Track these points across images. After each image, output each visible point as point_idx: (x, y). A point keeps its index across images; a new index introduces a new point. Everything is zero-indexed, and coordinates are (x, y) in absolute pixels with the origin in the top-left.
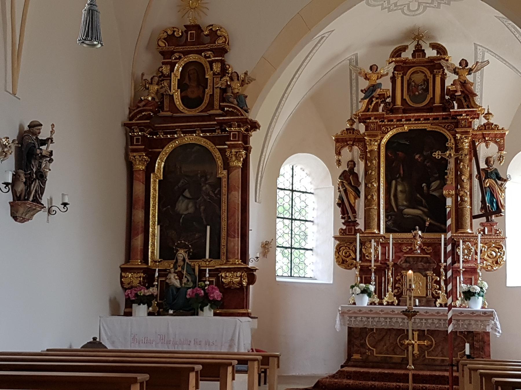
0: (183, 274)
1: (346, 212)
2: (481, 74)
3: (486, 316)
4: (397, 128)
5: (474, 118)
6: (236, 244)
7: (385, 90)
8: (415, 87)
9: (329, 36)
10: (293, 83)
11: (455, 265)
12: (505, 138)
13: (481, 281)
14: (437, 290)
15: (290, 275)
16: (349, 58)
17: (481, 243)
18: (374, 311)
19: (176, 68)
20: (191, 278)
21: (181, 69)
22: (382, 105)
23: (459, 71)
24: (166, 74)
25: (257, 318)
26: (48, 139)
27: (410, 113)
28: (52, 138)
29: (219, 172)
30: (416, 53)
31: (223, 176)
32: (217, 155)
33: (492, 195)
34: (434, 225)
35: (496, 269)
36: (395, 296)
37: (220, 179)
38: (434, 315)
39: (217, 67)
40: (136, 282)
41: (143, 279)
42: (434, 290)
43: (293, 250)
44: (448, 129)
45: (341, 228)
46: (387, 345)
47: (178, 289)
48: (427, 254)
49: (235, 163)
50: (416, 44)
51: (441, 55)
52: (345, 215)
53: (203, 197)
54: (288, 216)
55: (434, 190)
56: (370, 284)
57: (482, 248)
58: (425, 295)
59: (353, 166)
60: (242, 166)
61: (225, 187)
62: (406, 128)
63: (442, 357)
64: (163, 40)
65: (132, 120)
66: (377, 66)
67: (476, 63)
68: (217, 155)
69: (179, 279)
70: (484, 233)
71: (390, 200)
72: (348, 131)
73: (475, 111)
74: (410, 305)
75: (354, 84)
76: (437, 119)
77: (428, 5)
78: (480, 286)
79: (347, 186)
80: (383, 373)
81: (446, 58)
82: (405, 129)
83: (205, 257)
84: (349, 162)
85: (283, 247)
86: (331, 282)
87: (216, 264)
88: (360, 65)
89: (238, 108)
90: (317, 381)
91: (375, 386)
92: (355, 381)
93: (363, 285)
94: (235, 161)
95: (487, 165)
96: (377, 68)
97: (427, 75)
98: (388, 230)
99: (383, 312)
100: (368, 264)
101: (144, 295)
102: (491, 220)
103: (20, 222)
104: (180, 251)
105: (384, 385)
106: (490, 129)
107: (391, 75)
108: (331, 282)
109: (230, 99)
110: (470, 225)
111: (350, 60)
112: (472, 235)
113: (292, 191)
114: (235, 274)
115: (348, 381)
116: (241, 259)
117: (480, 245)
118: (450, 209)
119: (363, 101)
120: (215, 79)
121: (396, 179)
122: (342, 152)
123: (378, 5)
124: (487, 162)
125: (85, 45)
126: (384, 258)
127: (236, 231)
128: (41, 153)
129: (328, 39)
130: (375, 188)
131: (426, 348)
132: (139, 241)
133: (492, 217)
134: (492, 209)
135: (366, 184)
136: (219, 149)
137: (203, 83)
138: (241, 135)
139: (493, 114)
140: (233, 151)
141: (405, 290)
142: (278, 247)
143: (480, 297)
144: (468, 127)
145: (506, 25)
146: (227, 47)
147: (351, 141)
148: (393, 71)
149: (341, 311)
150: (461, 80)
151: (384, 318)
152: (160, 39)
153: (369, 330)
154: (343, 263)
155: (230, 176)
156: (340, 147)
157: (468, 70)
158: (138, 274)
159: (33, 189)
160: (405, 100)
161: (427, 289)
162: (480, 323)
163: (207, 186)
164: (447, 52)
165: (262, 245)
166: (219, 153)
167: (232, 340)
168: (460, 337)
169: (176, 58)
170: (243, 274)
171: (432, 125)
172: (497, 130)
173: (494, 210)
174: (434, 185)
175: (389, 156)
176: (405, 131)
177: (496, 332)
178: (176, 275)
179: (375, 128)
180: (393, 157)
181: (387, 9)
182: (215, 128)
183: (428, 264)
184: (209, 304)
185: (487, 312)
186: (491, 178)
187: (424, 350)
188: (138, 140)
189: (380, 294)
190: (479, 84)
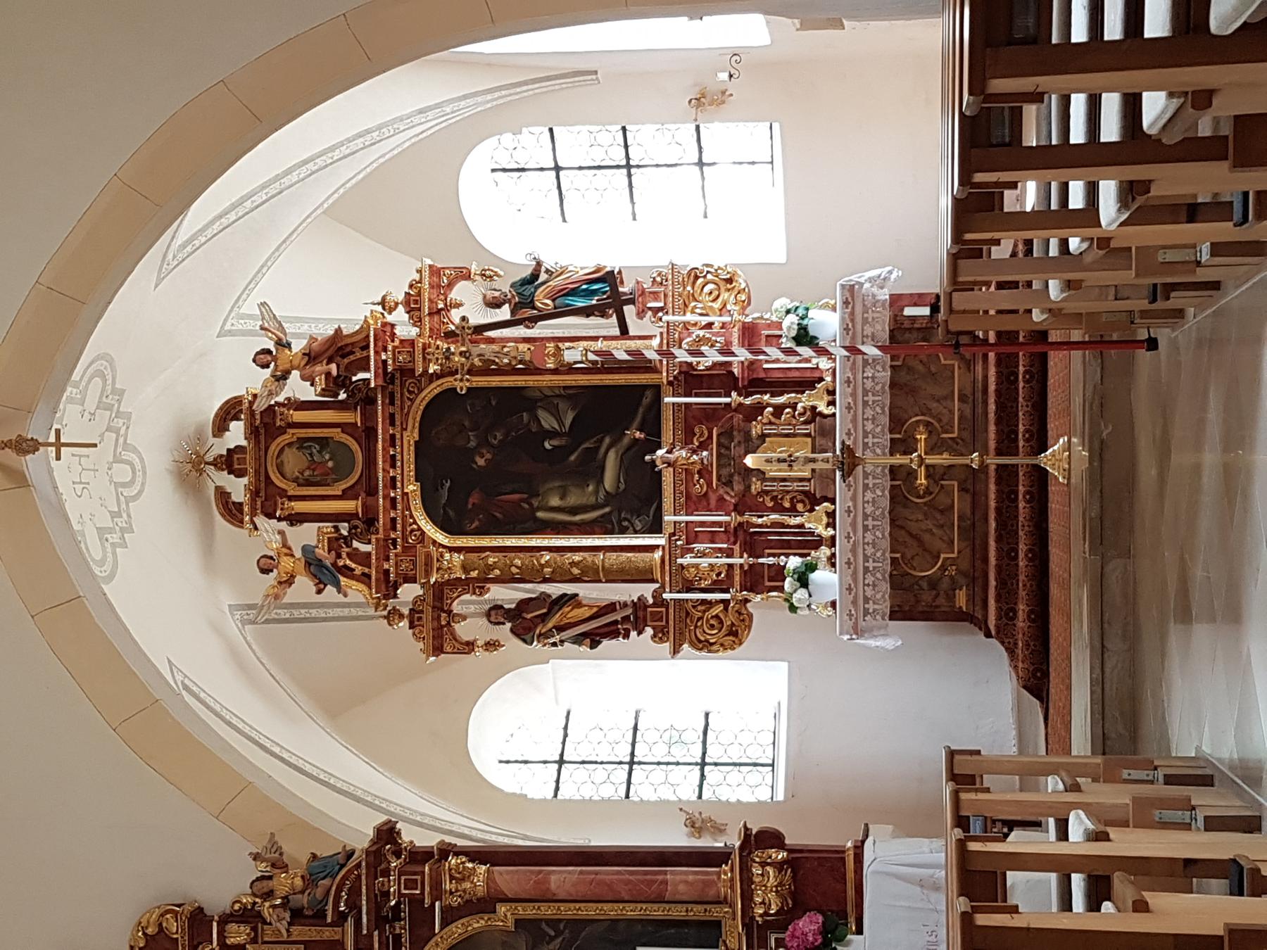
1: (612, 628)
2: (292, 323)
3: (853, 300)
4: (412, 508)
5: (393, 335)
6: (684, 877)
7: (318, 535)
8: (314, 470)
9: (181, 672)
10: (293, 760)
11: (736, 373)
12: (439, 266)
13: (772, 314)
14: (797, 413)
15: (771, 768)
16: (240, 625)
17: (684, 314)
18: (850, 555)
22: (356, 544)
23: (280, 368)
25: (866, 825)
27: (378, 479)
29: (501, 924)
30: (236, 466)
31: (512, 914)
32: (458, 929)
33: (573, 292)
34: (644, 420)
35: (746, 281)
36: (811, 510)
37: (518, 922)
38: (855, 416)
42: (795, 418)
43: (707, 760)
44: (416, 392)
45: (652, 638)
46: (931, 526)
48: (710, 437)
49: (479, 881)
50: (212, 467)
51: (241, 411)
52: (619, 629)
54: (622, 772)
56: (784, 567)
57: (694, 313)
58: (809, 440)
59: (501, 612)
60: (486, 865)
61: (539, 908)
62: (411, 487)
66: (262, 557)
67: (263, 332)
70: (661, 309)
71: (583, 523)
72: (416, 623)
73: (375, 333)
74: (828, 462)
75: (303, 613)
76: (392, 416)
77: (121, 440)
78: (784, 313)
79: (550, 625)
80: (996, 532)
81: (250, 398)
82: (414, 491)
84: (491, 622)
86: (786, 664)
87: (732, 932)
88: (259, 601)
90: (1025, 692)
91: (1030, 550)
92: (1021, 600)
93: (788, 584)
94: (472, 882)
95: (504, 304)
97: (287, 442)
98: (655, 527)
99: (851, 535)
100: (737, 571)
102: (631, 294)
105: (1026, 528)
106: (418, 298)
107: (283, 525)
109: (317, 896)
110: (642, 341)
111: (244, 622)
112: (665, 336)
114: (757, 880)
115: (1021, 615)
116: (721, 866)
117: (689, 317)
118: (589, 353)
120: (266, 939)
122: (466, 638)
123: (114, 554)
124: (495, 304)
126: (723, 536)
127: (649, 877)
129: (188, 674)
130: (555, 558)
131: (935, 438)
133: (622, 293)
134: (605, 293)
135: (545, 581)
138: (409, 868)
139: (384, 293)
141: (798, 486)
142: (700, 797)
143: (810, 316)
144: (414, 348)
145: (178, 265)
146: (188, 908)
147: (439, 616)
148: (275, 521)
149: (851, 635)
150: (303, 363)
153: (895, 569)
154: (735, 634)
156: (454, 642)
157: (280, 347)
161: (794, 435)
162: (870, 315)
165: (694, 836)
167: (921, 883)
168: (904, 359)
170: (757, 860)
171: (406, 429)
172: (421, 283)
173: (608, 289)
174: (547, 421)
175: (476, 527)
176: (419, 489)
177: (890, 278)
179: (410, 560)
180: (481, 516)
181: (125, 535)
182: (388, 938)
183: (735, 433)
184: (833, 945)
185: (844, 298)
186: (533, 295)
187: (940, 442)
189: (809, 543)
190: (313, 325)
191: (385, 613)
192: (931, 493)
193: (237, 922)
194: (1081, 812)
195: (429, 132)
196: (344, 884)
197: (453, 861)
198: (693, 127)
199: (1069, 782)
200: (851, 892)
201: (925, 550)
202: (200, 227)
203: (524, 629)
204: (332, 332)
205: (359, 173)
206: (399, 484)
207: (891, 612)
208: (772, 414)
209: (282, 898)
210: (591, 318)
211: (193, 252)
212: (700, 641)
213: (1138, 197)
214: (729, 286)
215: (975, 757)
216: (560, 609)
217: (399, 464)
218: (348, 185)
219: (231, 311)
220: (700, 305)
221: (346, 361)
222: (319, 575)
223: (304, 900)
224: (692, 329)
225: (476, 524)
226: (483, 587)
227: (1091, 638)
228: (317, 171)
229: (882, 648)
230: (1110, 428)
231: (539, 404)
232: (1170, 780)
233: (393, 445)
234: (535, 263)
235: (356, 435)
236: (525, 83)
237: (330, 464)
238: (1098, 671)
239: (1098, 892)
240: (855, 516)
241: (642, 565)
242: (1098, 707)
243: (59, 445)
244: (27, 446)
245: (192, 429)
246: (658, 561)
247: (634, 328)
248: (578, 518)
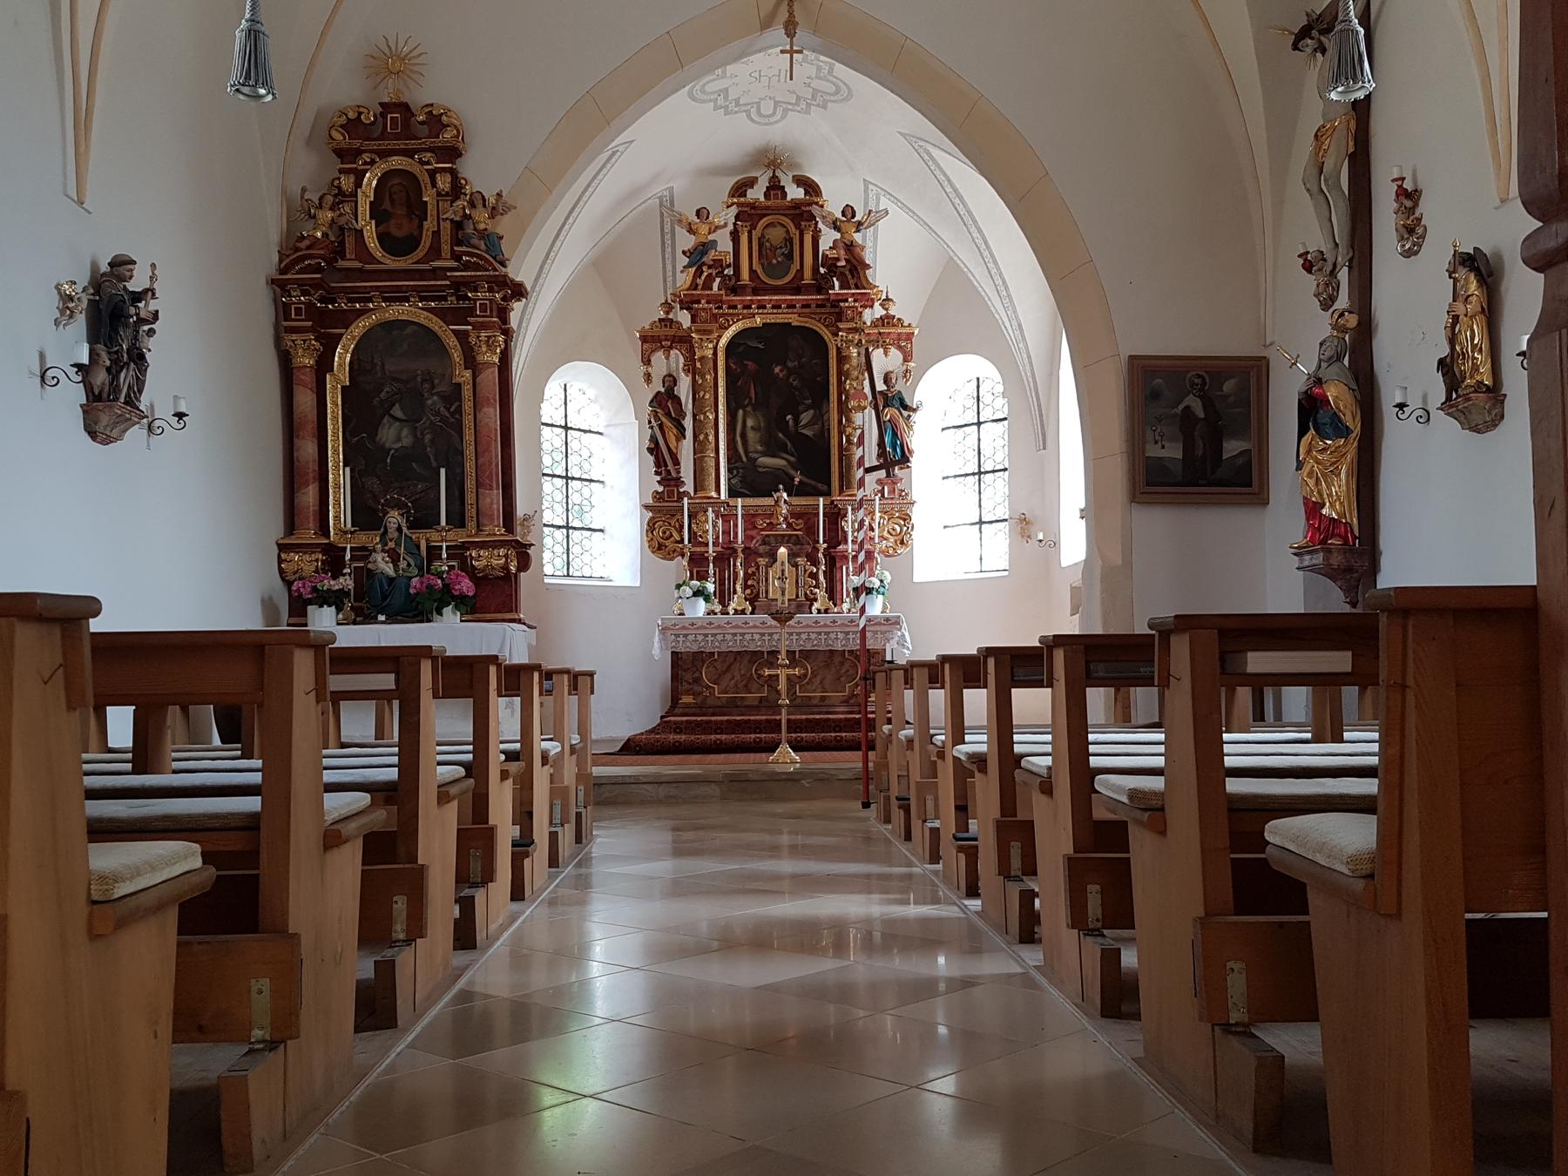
1: (662, 464)
5: (865, 307)
6: (495, 502)
8: (771, 250)
10: (564, 233)
17: (880, 512)
19: (366, 180)
20: (414, 559)
21: (375, 182)
22: (718, 280)
24: (347, 190)
26: (146, 291)
27: (765, 296)
32: (452, 342)
33: (895, 434)
34: (807, 484)
36: (746, 599)
37: (459, 385)
39: (445, 181)
40: (309, 569)
41: (322, 564)
47: (391, 580)
48: (795, 530)
53: (429, 419)
54: (560, 471)
55: (805, 426)
58: (794, 597)
59: (672, 383)
61: (469, 400)
64: (340, 129)
65: (286, 274)
67: (867, 212)
68: (452, 342)
69: (392, 562)
70: (883, 495)
77: (790, 107)
79: (663, 419)
84: (665, 377)
85: (552, 526)
86: (638, 585)
89: (488, 257)
91: (721, 741)
94: (486, 352)
98: (733, 493)
100: (703, 549)
101: (329, 590)
103: (101, 443)
107: (731, 227)
108: (638, 585)
113: (566, 428)
114: (495, 552)
115: (677, 737)
117: (878, 515)
119: (687, 270)
120: (440, 203)
121: (744, 408)
122: (653, 359)
123: (710, 101)
124: (887, 379)
125: (241, 97)
128: (137, 315)
131: (797, 680)
134: (894, 457)
135: (694, 416)
136: (452, 331)
137: (418, 211)
138: (495, 306)
142: (545, 525)
143: (879, 596)
150: (845, 241)
151: (732, 634)
152: (334, 126)
154: (659, 549)
158: (313, 555)
159: (124, 384)
163: (435, 398)
169: (365, 162)
170: (509, 552)
174: (806, 417)
183: (799, 547)
186: (893, 406)
188: (298, 311)
189: (723, 596)
191: (669, 301)
192: (758, 678)
193: (452, 182)
194: (560, 749)
195: (1006, 334)
196: (482, 260)
197: (501, 338)
198: (1006, 517)
199: (577, 747)
200: (489, 616)
201: (720, 676)
202: (941, 164)
203: (661, 401)
204: (867, 262)
205: (977, 281)
206: (760, 311)
207: (677, 653)
208: (811, 572)
209: (470, 214)
210: (877, 448)
211: (924, 161)
212: (654, 524)
213: (975, 765)
214: (898, 542)
216: (676, 427)
217: (775, 311)
218: (970, 275)
219: (882, 189)
220: (885, 522)
222: (696, 252)
223: (470, 230)
224: (869, 517)
225: (734, 366)
226: (689, 372)
227: (666, 775)
228: (980, 251)
229: (653, 647)
230: (807, 785)
231: (818, 411)
232: (579, 815)
233: (788, 307)
234: (915, 407)
235: (795, 280)
236: (1038, 399)
237: (774, 261)
238: (644, 780)
239: (511, 756)
240: (743, 628)
241: (707, 484)
242: (620, 780)
243: (791, 52)
244: (790, 28)
245: (797, 160)
246: (709, 495)
247: (871, 479)
248: (738, 439)
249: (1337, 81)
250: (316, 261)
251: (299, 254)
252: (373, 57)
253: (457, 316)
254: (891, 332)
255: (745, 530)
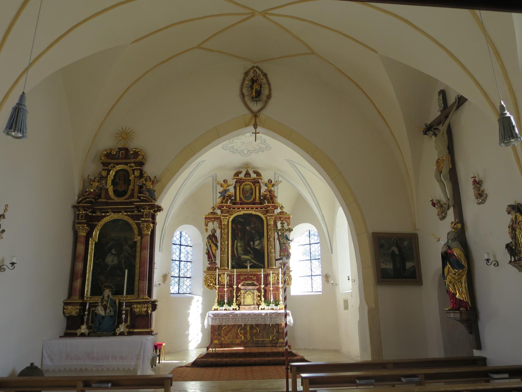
0: (107, 306)
5: (275, 209)
6: (145, 285)
8: (246, 192)
10: (182, 187)
15: (178, 293)
19: (111, 172)
22: (230, 200)
28: (4, 215)
32: (135, 226)
39: (137, 173)
47: (103, 317)
50: (246, 170)
54: (178, 259)
55: (257, 246)
63: (263, 338)
68: (135, 226)
72: (212, 214)
75: (215, 189)
77: (252, 152)
79: (211, 243)
83: (123, 294)
84: (212, 230)
85: (174, 277)
88: (218, 179)
96: (227, 181)
98: (233, 267)
104: (106, 290)
107: (234, 185)
114: (143, 305)
116: (147, 295)
120: (135, 180)
121: (237, 240)
132: (78, 283)
135: (221, 242)
137: (128, 182)
140: (145, 224)
142: (172, 277)
146: (144, 161)
148: (235, 183)
155: (142, 240)
158: (76, 307)
160: (241, 198)
163: (127, 246)
164: (261, 175)
166: (136, 226)
174: (257, 243)
178: (102, 307)
188: (82, 216)
191: (214, 207)
193: (140, 173)
197: (152, 225)
215: (170, 385)
221: (270, 199)
225: (234, 227)
233: (251, 209)
240: (236, 316)
243: (256, 133)
244: (255, 126)
249: (504, 138)
250: (91, 199)
251: (85, 197)
252: (118, 134)
253: (138, 218)
254: (284, 217)
255: (237, 280)
